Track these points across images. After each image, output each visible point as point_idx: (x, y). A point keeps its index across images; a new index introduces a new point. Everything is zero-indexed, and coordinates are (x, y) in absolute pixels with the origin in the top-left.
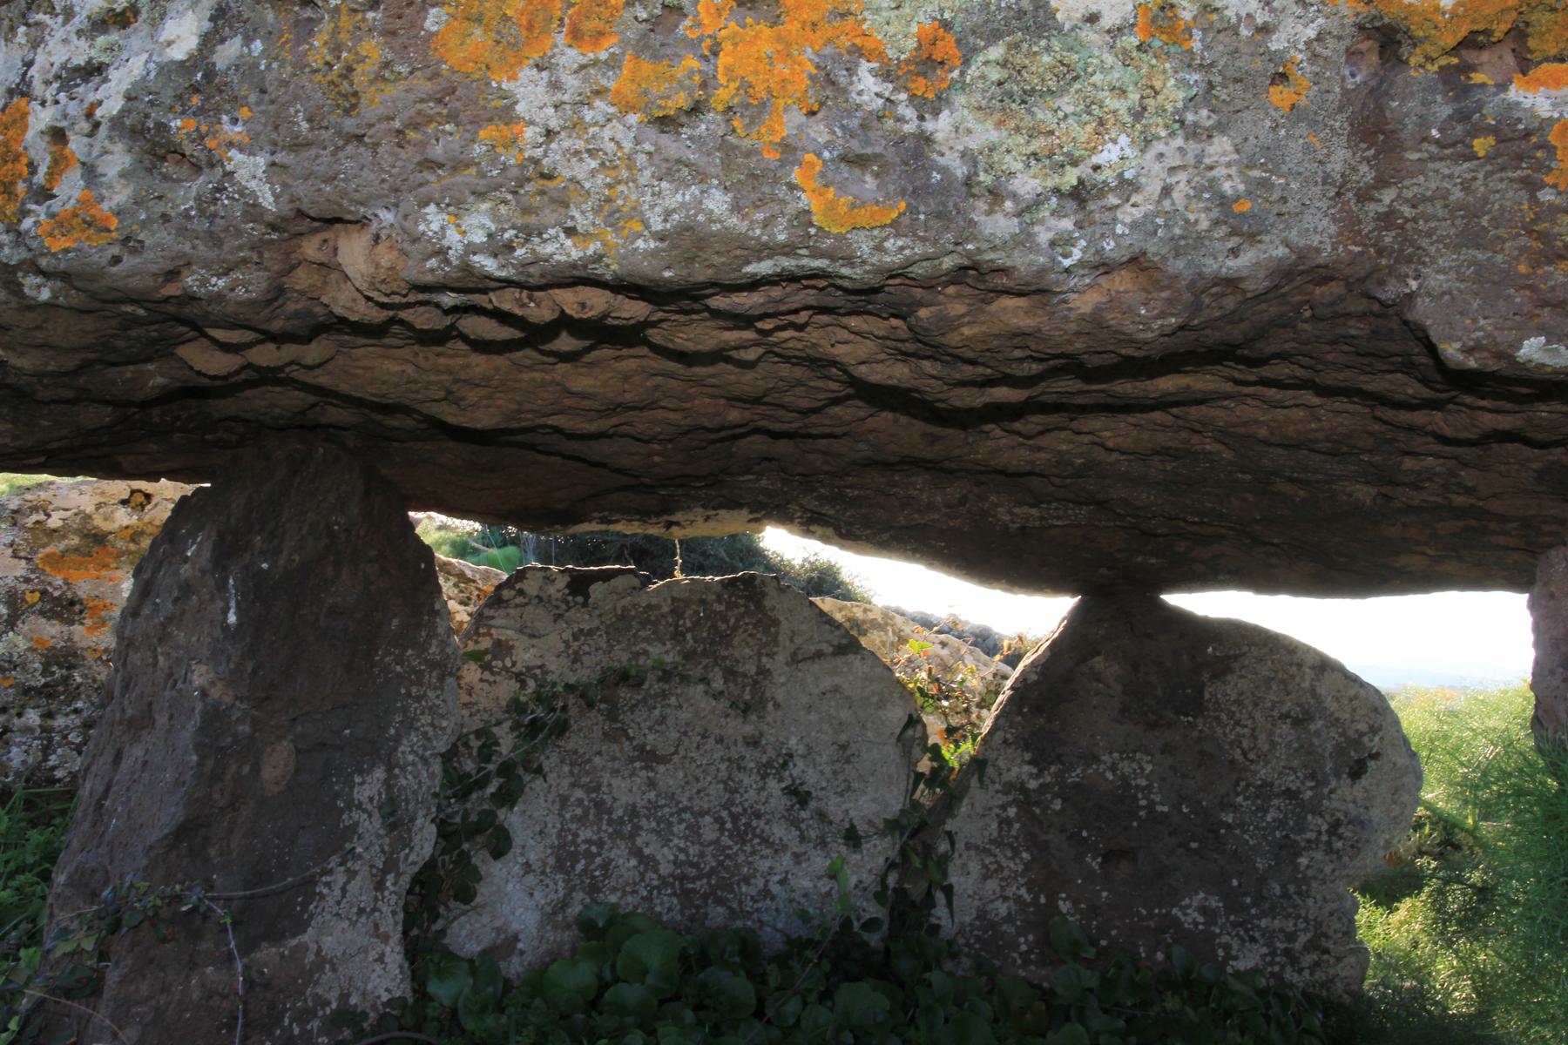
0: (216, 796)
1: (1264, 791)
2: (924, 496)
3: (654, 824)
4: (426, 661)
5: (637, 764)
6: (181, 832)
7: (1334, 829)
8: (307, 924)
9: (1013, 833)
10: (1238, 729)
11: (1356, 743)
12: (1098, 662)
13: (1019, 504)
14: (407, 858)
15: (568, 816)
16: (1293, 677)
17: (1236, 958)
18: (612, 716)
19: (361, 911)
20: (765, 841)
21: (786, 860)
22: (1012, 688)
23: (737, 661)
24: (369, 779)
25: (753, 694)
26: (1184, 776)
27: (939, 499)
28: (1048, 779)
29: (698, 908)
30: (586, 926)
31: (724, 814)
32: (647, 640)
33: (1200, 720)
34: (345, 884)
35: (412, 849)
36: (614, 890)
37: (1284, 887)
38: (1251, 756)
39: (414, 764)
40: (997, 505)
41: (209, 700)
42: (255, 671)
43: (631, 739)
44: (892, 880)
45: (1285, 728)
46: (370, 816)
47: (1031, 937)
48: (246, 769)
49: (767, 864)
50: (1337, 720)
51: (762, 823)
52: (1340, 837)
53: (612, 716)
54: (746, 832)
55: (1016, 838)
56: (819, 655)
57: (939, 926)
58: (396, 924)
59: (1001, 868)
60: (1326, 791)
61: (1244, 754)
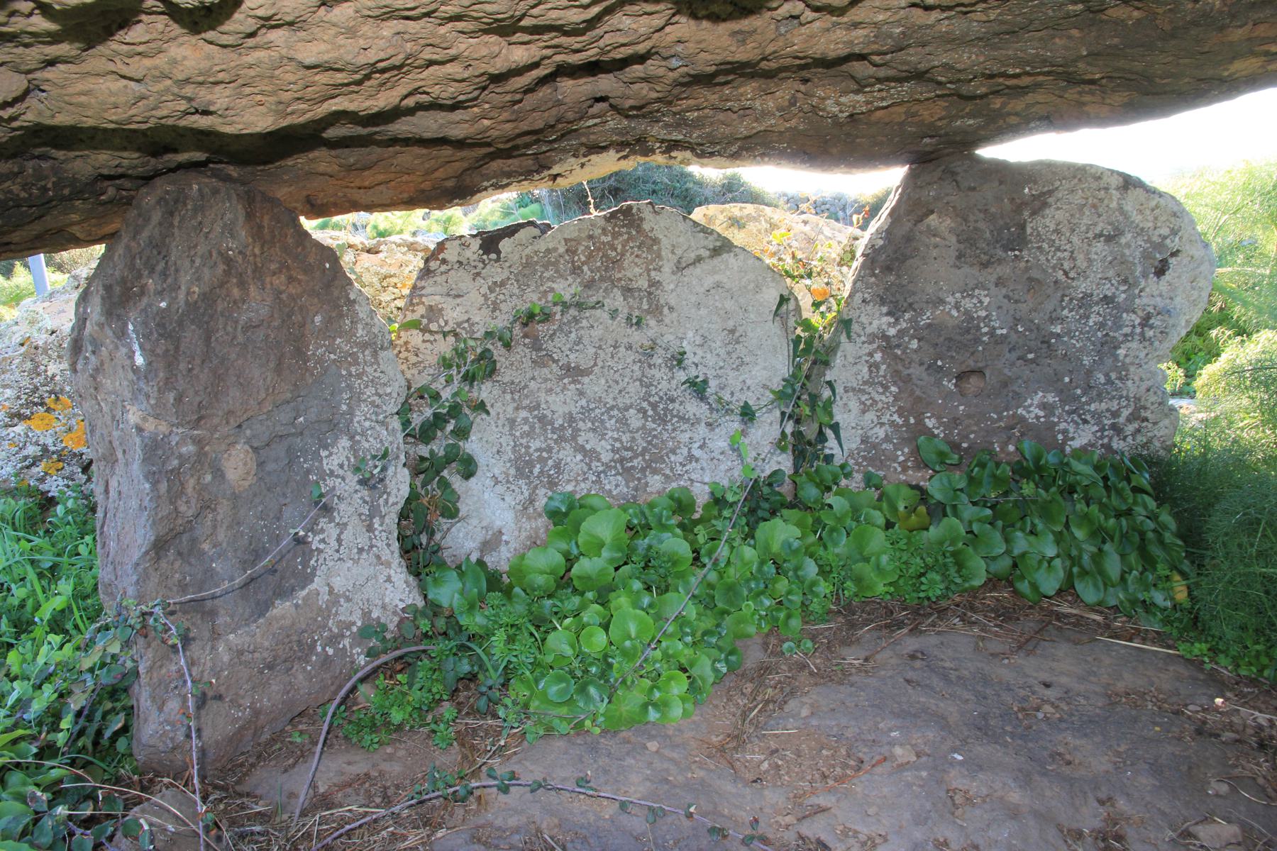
0: (183, 508)
1: (1085, 301)
2: (757, 104)
3: (589, 425)
4: (357, 344)
5: (566, 381)
6: (159, 547)
7: (1145, 322)
8: (313, 574)
9: (881, 373)
10: (1059, 254)
11: (1160, 246)
12: (933, 220)
13: (845, 92)
14: (387, 501)
15: (518, 434)
16: (1101, 200)
17: (1073, 439)
18: (536, 347)
19: (361, 550)
20: (682, 418)
21: (702, 429)
22: (863, 255)
23: (631, 280)
24: (335, 450)
25: (650, 304)
26: (1016, 302)
27: (771, 104)
28: (904, 325)
29: (639, 479)
30: (555, 516)
31: (645, 405)
32: (551, 279)
33: (1025, 253)
34: (339, 535)
35: (389, 494)
36: (569, 481)
37: (1107, 375)
38: (1072, 275)
39: (372, 428)
40: (824, 99)
41: (146, 434)
42: (179, 399)
43: (555, 361)
44: (789, 428)
45: (1099, 246)
46: (343, 479)
47: (906, 450)
48: (208, 478)
49: (687, 435)
50: (1142, 229)
51: (677, 405)
52: (1151, 327)
53: (536, 347)
54: (665, 415)
55: (884, 377)
56: (699, 259)
57: (832, 455)
58: (392, 553)
59: (875, 402)
60: (1137, 291)
61: (1066, 273)
